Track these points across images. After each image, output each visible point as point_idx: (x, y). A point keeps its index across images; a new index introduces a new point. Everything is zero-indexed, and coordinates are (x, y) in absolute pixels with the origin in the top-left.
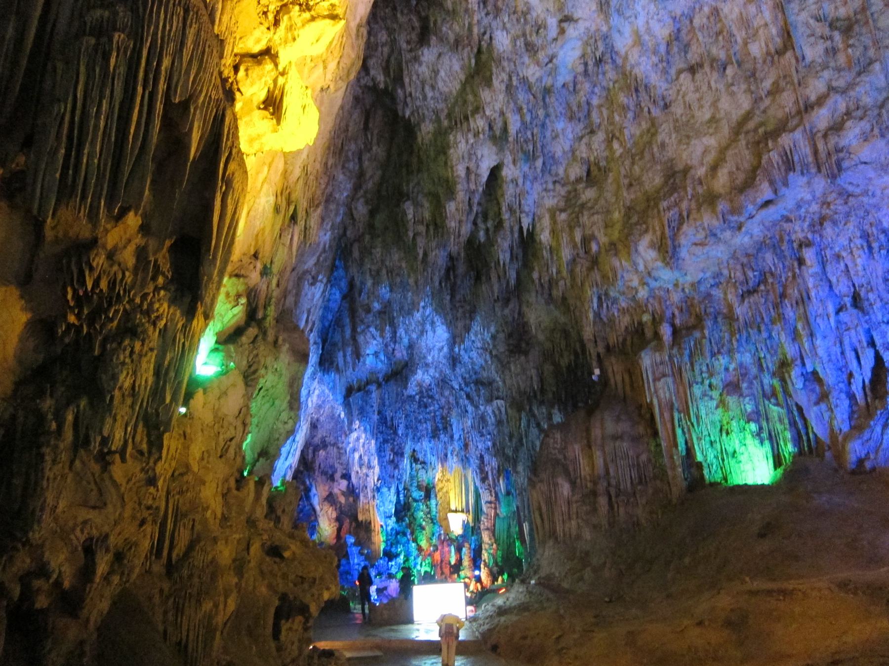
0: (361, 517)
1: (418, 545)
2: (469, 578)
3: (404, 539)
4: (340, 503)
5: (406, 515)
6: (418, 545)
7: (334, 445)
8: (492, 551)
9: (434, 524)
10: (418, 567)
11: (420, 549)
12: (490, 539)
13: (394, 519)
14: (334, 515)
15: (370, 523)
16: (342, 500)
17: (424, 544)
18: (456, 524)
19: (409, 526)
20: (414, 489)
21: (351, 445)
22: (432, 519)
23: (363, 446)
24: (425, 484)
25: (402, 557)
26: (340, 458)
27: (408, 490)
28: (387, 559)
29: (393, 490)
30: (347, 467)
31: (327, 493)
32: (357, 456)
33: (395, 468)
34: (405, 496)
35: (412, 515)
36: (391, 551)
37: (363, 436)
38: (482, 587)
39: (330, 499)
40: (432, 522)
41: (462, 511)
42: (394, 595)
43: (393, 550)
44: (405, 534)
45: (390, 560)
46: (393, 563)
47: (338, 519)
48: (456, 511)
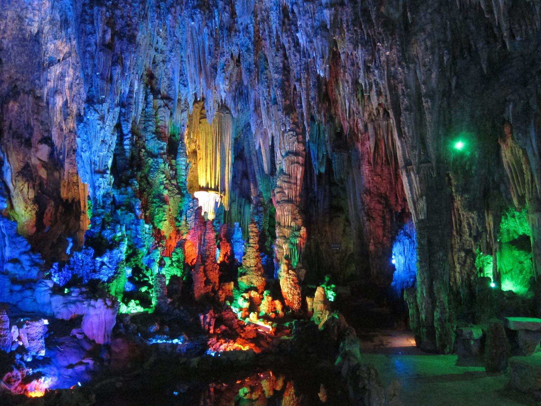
0: (64, 194)
1: (154, 228)
2: (256, 289)
3: (131, 217)
4: (40, 177)
5: (133, 176)
6: (154, 228)
7: (28, 93)
8: (297, 241)
9: (183, 196)
10: (156, 268)
11: (158, 235)
12: (294, 219)
13: (110, 177)
14: (32, 195)
15: (79, 202)
16: (43, 173)
17: (165, 227)
18: (208, 202)
19: (140, 194)
20: (149, 136)
21: (51, 84)
22: (179, 188)
23: (71, 88)
24: (168, 135)
25: (124, 248)
26: (38, 113)
27: (140, 137)
28: (92, 251)
29: (110, 122)
30: (46, 125)
31: (22, 165)
32: (59, 101)
33: (114, 64)
34: (133, 145)
35: (146, 177)
36: (101, 237)
37: (71, 71)
38: (285, 308)
39: (27, 173)
40: (180, 193)
41: (216, 189)
42: (100, 340)
43: (107, 233)
44: (130, 208)
45: (99, 253)
46: (106, 259)
47: (37, 200)
48: (207, 189)
